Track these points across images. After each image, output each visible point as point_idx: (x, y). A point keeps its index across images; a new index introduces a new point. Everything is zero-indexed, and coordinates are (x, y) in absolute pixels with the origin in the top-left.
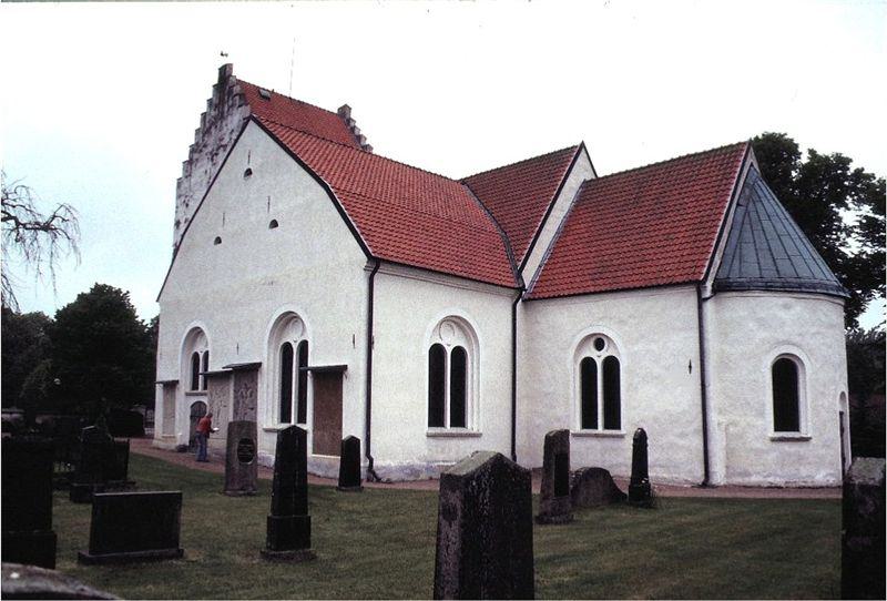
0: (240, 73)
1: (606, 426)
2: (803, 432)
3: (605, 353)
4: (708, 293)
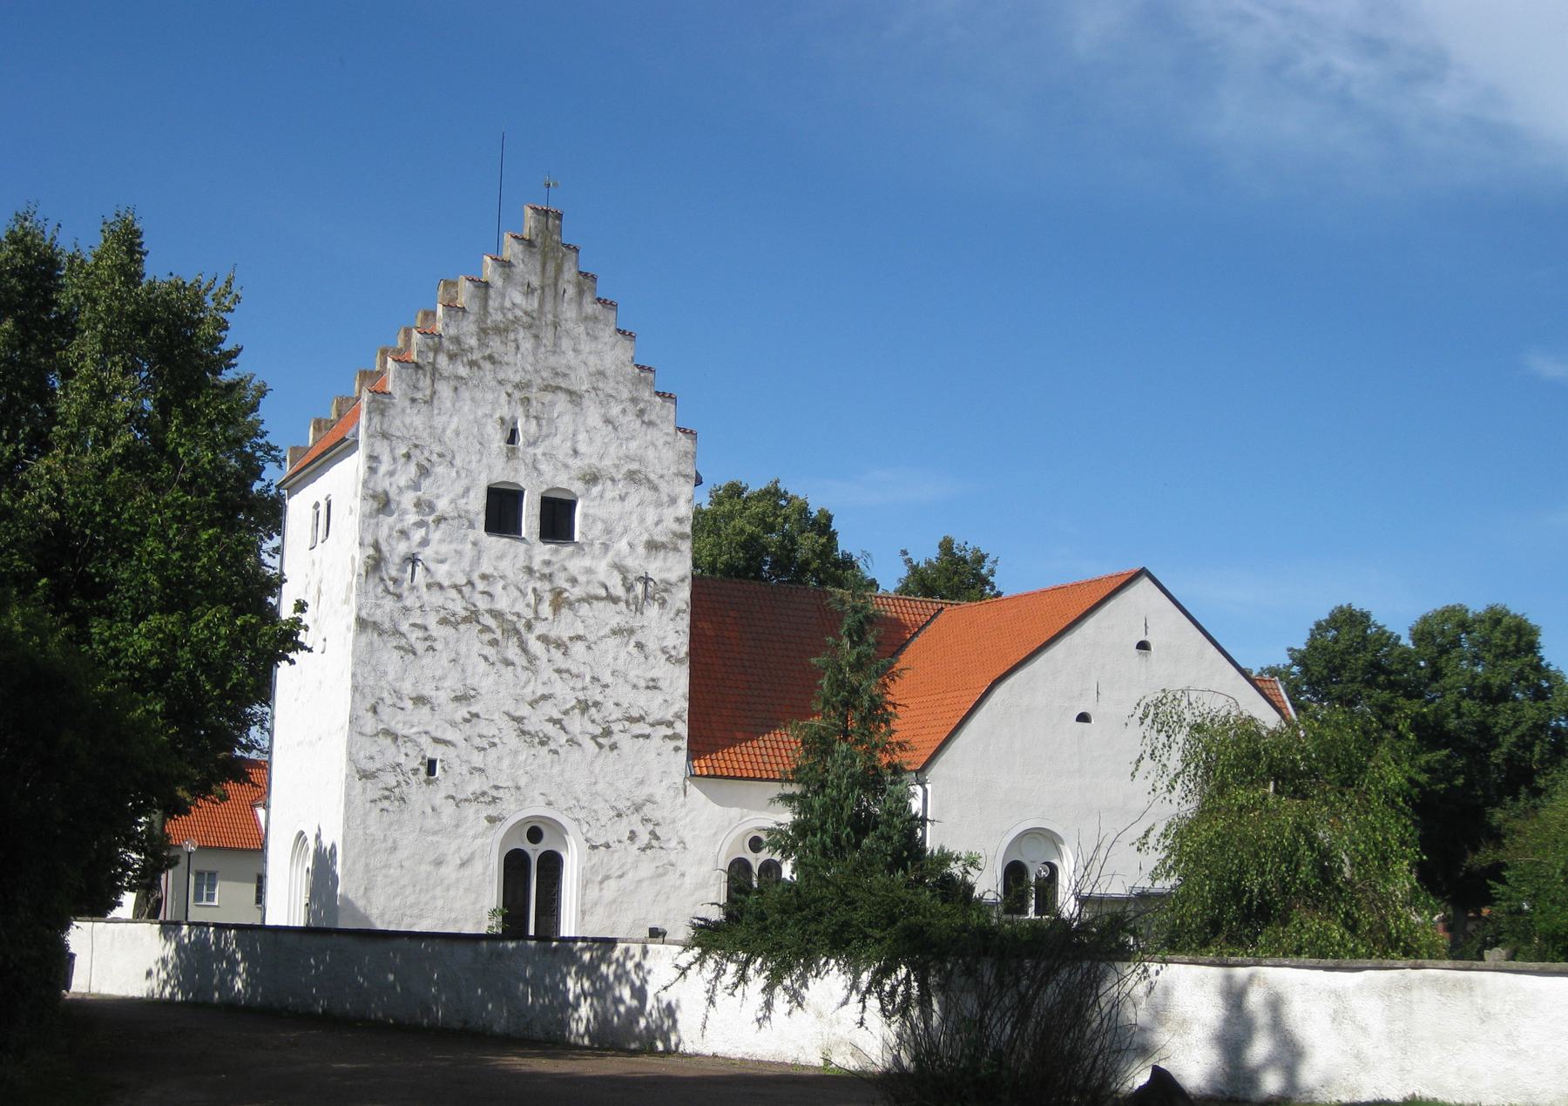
3: (542, 847)
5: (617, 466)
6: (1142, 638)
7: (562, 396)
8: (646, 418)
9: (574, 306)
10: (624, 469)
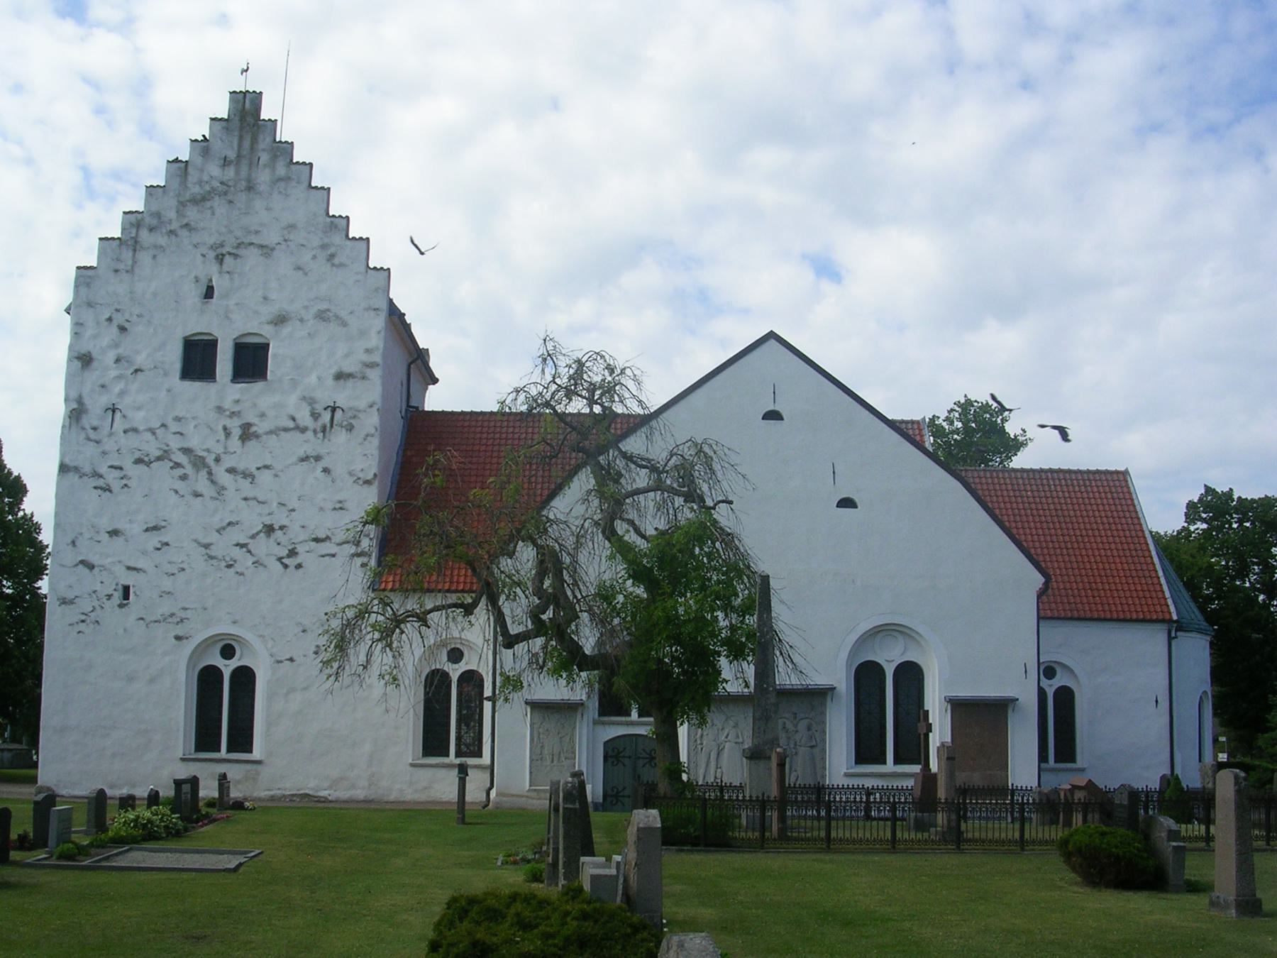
2: (257, 753)
3: (234, 663)
5: (306, 307)
6: (771, 408)
7: (255, 251)
8: (336, 261)
10: (314, 310)
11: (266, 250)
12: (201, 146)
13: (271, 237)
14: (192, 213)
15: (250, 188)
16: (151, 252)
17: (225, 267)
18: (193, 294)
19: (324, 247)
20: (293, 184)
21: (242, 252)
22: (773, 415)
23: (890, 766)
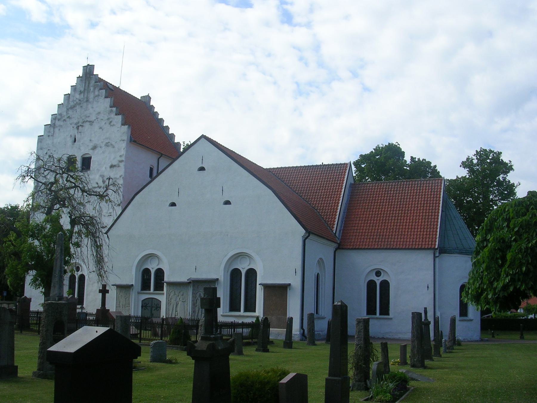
0: (101, 72)
1: (246, 310)
2: (391, 316)
3: (381, 278)
4: (437, 255)
5: (102, 142)
6: (201, 166)
7: (88, 123)
8: (112, 124)
9: (93, 93)
10: (104, 143)
11: (91, 123)
12: (74, 88)
13: (93, 118)
14: (70, 112)
15: (87, 101)
16: (59, 128)
17: (79, 131)
18: (70, 141)
19: (108, 119)
20: (100, 97)
21: (84, 124)
22: (202, 169)
23: (242, 313)
